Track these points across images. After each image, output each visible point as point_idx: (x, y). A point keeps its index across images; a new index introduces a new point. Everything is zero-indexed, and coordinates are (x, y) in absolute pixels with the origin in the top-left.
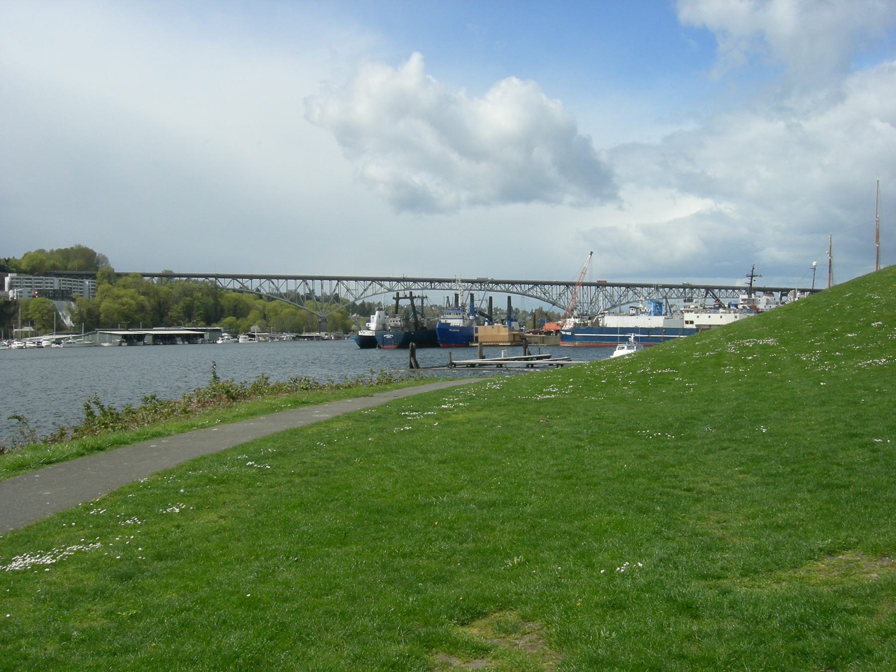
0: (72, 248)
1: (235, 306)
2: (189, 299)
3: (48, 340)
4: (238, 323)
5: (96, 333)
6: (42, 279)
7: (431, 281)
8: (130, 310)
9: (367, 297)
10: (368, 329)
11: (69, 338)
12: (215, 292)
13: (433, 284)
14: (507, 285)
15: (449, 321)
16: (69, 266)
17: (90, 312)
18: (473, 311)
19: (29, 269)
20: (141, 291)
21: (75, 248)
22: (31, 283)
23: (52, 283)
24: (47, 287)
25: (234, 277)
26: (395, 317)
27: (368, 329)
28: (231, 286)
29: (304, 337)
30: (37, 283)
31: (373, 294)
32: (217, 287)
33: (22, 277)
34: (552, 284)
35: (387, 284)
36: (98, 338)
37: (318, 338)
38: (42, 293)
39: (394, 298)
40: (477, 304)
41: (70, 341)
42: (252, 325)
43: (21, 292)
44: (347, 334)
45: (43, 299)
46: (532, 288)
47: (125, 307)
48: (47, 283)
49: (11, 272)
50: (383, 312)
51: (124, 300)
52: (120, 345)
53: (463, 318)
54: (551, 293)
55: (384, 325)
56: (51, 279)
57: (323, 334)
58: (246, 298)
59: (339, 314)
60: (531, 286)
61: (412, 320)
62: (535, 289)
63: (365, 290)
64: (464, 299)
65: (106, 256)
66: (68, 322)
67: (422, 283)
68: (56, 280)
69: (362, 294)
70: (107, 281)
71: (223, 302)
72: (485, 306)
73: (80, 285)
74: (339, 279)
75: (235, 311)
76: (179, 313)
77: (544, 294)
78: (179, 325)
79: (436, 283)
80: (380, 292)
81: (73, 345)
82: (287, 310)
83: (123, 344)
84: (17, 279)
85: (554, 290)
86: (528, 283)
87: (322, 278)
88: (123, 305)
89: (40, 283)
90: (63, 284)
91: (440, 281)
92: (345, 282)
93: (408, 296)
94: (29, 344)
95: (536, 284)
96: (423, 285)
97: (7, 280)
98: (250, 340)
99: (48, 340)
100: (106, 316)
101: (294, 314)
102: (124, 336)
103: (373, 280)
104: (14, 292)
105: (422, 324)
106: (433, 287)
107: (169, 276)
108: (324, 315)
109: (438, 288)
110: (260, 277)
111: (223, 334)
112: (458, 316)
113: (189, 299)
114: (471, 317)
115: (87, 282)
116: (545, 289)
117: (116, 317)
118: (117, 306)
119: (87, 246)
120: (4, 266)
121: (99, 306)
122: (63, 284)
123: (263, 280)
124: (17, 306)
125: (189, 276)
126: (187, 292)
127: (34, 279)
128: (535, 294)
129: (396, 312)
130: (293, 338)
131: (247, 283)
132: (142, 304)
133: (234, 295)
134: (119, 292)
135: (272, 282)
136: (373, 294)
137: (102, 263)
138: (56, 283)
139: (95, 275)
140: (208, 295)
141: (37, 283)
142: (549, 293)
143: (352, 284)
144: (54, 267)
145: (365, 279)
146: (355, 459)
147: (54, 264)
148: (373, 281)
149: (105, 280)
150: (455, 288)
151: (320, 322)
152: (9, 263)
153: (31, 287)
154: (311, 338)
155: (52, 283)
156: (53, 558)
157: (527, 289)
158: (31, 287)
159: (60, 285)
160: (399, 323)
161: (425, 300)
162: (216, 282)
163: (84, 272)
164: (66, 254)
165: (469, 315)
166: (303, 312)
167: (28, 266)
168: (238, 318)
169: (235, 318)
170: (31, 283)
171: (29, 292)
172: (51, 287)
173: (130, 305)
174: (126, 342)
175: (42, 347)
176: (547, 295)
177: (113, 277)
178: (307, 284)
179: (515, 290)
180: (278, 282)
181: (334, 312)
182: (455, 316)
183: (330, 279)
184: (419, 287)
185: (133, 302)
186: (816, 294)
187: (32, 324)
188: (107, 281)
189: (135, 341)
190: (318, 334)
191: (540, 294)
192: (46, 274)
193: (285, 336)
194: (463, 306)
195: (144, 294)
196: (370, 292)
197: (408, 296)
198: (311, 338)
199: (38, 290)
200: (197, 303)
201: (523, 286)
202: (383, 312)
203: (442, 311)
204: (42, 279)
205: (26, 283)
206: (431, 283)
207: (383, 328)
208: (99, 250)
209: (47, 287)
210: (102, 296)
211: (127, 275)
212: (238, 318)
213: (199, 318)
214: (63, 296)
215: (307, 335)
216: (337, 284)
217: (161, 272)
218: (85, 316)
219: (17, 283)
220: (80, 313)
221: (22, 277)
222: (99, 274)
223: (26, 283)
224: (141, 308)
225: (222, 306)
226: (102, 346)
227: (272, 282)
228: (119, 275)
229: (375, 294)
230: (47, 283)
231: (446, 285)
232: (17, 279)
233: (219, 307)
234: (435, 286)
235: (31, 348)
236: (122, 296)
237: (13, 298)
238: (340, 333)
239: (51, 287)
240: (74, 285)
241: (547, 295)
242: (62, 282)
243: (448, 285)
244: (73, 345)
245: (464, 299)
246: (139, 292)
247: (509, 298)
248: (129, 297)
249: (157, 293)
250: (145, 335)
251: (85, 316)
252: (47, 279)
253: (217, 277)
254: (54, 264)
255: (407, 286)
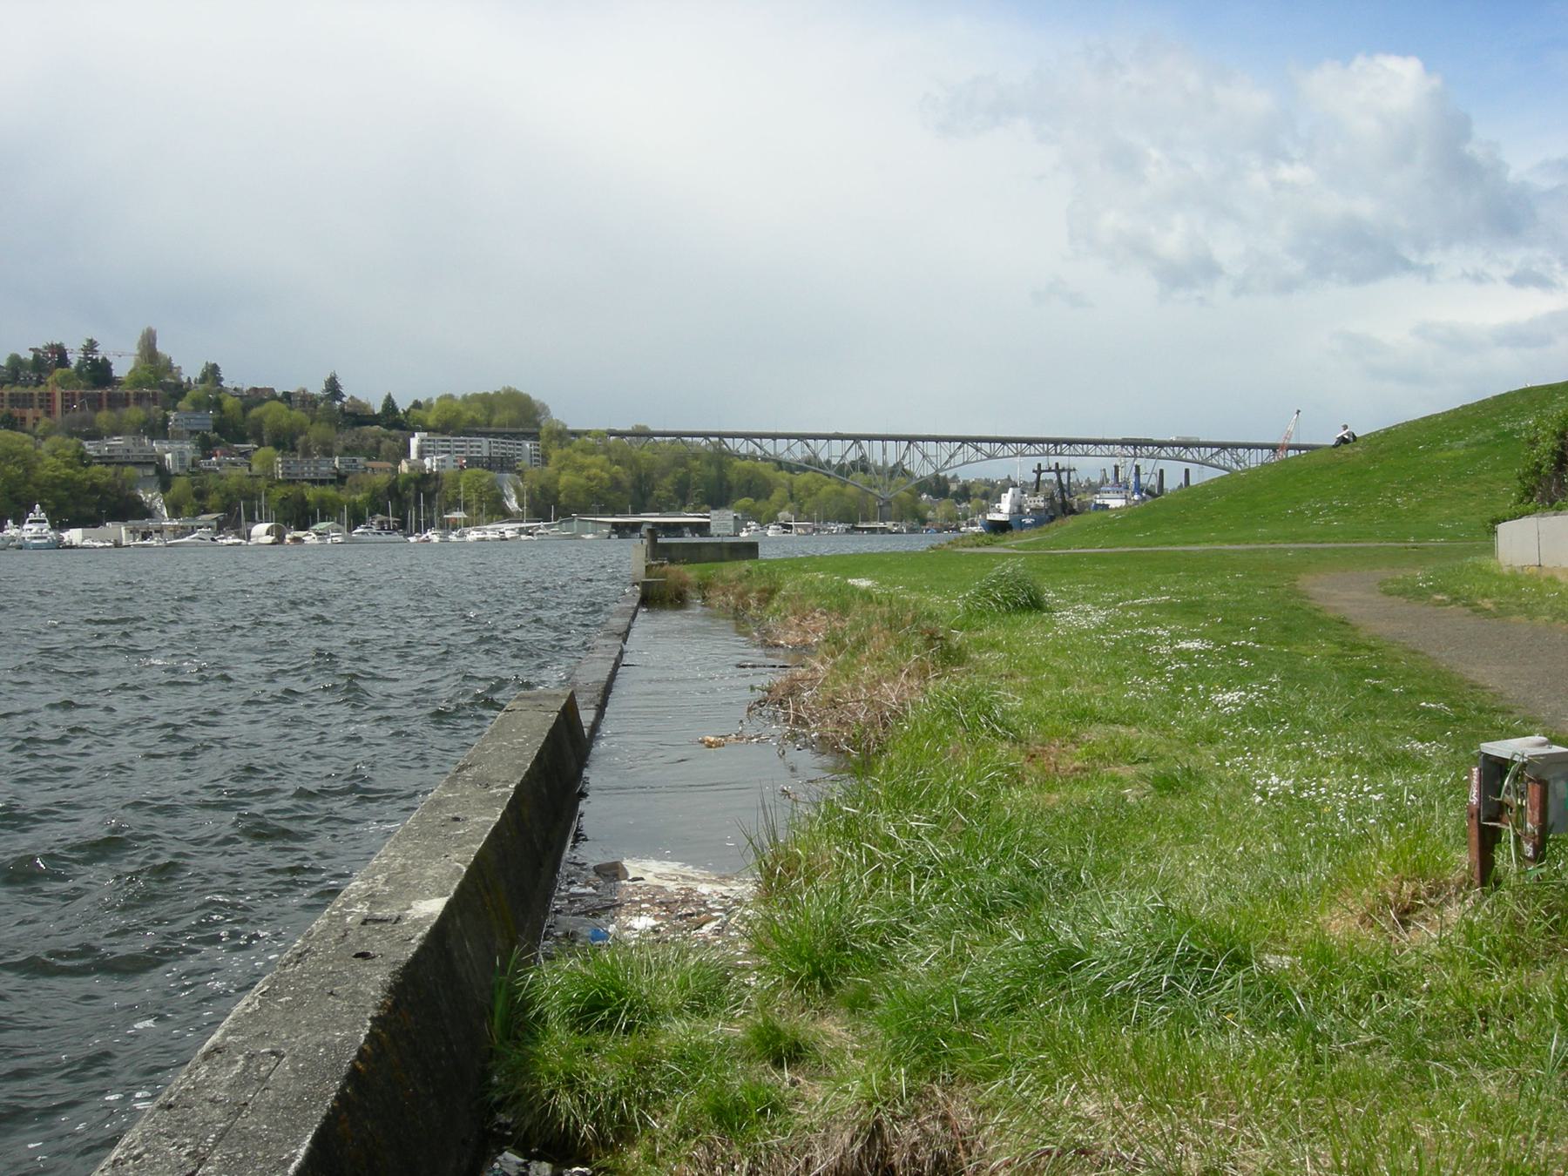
0: (497, 393)
1: (749, 482)
2: (682, 470)
3: (513, 530)
4: (758, 506)
5: (573, 520)
6: (465, 441)
7: (1056, 442)
8: (601, 488)
9: (955, 467)
10: (999, 511)
11: (539, 527)
12: (721, 458)
13: (1058, 447)
14: (1176, 449)
15: (1107, 502)
16: (496, 419)
17: (544, 490)
18: (1139, 488)
19: (440, 426)
20: (614, 458)
21: (502, 393)
22: (449, 446)
23: (479, 447)
24: (472, 452)
25: (747, 436)
26: (1036, 496)
27: (999, 511)
28: (743, 451)
29: (863, 529)
30: (457, 446)
31: (964, 463)
32: (723, 453)
33: (436, 438)
34: (1249, 447)
35: (985, 446)
36: (575, 526)
37: (883, 531)
38: (473, 462)
39: (1034, 471)
40: (1143, 479)
41: (540, 531)
42: (779, 511)
43: (443, 461)
44: (925, 525)
45: (477, 470)
46: (1217, 453)
47: (594, 483)
48: (472, 447)
49: (418, 431)
50: (1018, 490)
51: (593, 471)
52: (609, 538)
53: (1126, 498)
54: (1247, 462)
55: (1020, 507)
56: (476, 441)
57: (889, 525)
58: (767, 470)
59: (907, 494)
60: (1215, 450)
61: (1058, 500)
62: (1222, 454)
63: (951, 457)
64: (1127, 473)
65: (547, 403)
66: (512, 504)
67: (1014, 445)
68: (484, 441)
69: (946, 463)
70: (558, 442)
71: (733, 477)
72: (1154, 481)
73: (518, 450)
74: (911, 440)
75: (749, 489)
76: (669, 491)
77: (1237, 463)
78: (671, 509)
79: (1064, 446)
80: (975, 459)
81: (545, 537)
82: (827, 488)
83: (613, 536)
84: (429, 441)
85: (1253, 456)
86: (1212, 445)
87: (884, 438)
88: (588, 478)
89: (462, 446)
90: (495, 447)
91: (1070, 442)
92: (920, 443)
93: (1053, 468)
94: (490, 535)
95: (1223, 446)
96: (1017, 449)
97: (414, 443)
98: (784, 532)
99: (513, 530)
100: (567, 496)
101: (839, 494)
102: (615, 525)
103: (964, 440)
104: (432, 461)
105: (1071, 506)
106: (1058, 451)
107: (642, 434)
108: (887, 496)
109: (1067, 453)
110: (788, 437)
111: (749, 523)
112: (1119, 496)
113: (682, 470)
114: (1136, 497)
115: (528, 445)
116: (1238, 455)
117: (581, 497)
118: (582, 481)
119: (531, 395)
120: (403, 422)
121: (557, 482)
122: (495, 447)
123: (793, 441)
124: (439, 482)
125: (679, 435)
126: (680, 461)
127: (439, 440)
128: (1222, 463)
129: (1037, 489)
130: (847, 529)
131: (768, 444)
132: (616, 478)
133: (746, 464)
134: (582, 460)
135: (808, 445)
136: (964, 463)
137: (540, 415)
138: (484, 447)
139: (538, 434)
140: (709, 465)
141: (457, 446)
142: (1244, 462)
143: (931, 447)
144: (474, 422)
145: (951, 439)
146: (303, 1068)
147: (473, 417)
148: (963, 443)
149: (553, 442)
150: (1093, 453)
151: (880, 507)
152: (410, 417)
153: (449, 452)
154: (873, 531)
155: (479, 447)
156: (310, 934)
157: (1208, 455)
158: (449, 452)
159: (490, 448)
160: (1042, 504)
161: (1072, 474)
162: (720, 445)
163: (521, 430)
164: (488, 402)
165: (1133, 494)
166: (850, 490)
167: (438, 420)
168: (757, 499)
169: (752, 500)
170: (449, 446)
171: (455, 461)
172: (478, 452)
173: (602, 479)
174: (616, 533)
175: (506, 539)
176: (1242, 464)
177: (563, 436)
178: (860, 447)
179: (1190, 457)
180: (775, 445)
181: (901, 491)
182: (1116, 495)
183: (897, 439)
184: (758, 441)
185: (605, 475)
186: (1316, 453)
187: (466, 508)
188: (558, 442)
189: (627, 532)
190: (882, 525)
191: (1229, 463)
192: (465, 433)
193: (834, 527)
194: (1126, 482)
195: (618, 463)
196: (958, 459)
197: (1053, 468)
198: (873, 531)
199: (466, 458)
200: (695, 477)
201: (1202, 449)
202: (1018, 490)
203: (1094, 489)
204: (465, 441)
205: (442, 446)
206: (1056, 445)
207: (1018, 510)
208: (537, 394)
209: (472, 452)
210: (559, 466)
211: (587, 433)
212: (757, 499)
213: (698, 500)
214: (502, 466)
215: (865, 526)
216: (908, 448)
217: (630, 429)
218: (538, 497)
219: (429, 446)
220: (530, 492)
221: (436, 438)
222: (543, 433)
223: (442, 446)
224: (616, 484)
225: (729, 482)
226: (583, 538)
227: (808, 445)
228: (575, 434)
229: (967, 462)
230: (472, 447)
231: (1079, 448)
232: (429, 441)
233: (725, 483)
234: (1061, 450)
235: (495, 540)
236: (588, 467)
237: (431, 470)
238: (916, 524)
239: (478, 452)
240: (510, 449)
241: (1242, 464)
242: (493, 445)
243: (1043, 448)
244: (545, 537)
245: (1127, 473)
246: (611, 460)
247: (1187, 471)
248: (598, 468)
249: (635, 461)
250: (642, 523)
251: (538, 497)
252: (472, 441)
253: (721, 436)
254: (473, 417)
255: (1017, 449)
